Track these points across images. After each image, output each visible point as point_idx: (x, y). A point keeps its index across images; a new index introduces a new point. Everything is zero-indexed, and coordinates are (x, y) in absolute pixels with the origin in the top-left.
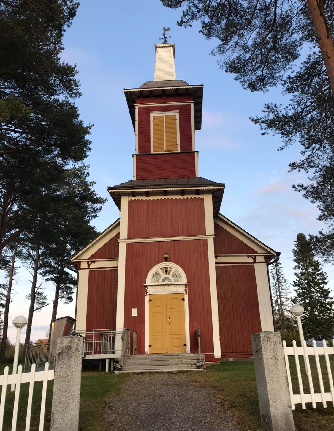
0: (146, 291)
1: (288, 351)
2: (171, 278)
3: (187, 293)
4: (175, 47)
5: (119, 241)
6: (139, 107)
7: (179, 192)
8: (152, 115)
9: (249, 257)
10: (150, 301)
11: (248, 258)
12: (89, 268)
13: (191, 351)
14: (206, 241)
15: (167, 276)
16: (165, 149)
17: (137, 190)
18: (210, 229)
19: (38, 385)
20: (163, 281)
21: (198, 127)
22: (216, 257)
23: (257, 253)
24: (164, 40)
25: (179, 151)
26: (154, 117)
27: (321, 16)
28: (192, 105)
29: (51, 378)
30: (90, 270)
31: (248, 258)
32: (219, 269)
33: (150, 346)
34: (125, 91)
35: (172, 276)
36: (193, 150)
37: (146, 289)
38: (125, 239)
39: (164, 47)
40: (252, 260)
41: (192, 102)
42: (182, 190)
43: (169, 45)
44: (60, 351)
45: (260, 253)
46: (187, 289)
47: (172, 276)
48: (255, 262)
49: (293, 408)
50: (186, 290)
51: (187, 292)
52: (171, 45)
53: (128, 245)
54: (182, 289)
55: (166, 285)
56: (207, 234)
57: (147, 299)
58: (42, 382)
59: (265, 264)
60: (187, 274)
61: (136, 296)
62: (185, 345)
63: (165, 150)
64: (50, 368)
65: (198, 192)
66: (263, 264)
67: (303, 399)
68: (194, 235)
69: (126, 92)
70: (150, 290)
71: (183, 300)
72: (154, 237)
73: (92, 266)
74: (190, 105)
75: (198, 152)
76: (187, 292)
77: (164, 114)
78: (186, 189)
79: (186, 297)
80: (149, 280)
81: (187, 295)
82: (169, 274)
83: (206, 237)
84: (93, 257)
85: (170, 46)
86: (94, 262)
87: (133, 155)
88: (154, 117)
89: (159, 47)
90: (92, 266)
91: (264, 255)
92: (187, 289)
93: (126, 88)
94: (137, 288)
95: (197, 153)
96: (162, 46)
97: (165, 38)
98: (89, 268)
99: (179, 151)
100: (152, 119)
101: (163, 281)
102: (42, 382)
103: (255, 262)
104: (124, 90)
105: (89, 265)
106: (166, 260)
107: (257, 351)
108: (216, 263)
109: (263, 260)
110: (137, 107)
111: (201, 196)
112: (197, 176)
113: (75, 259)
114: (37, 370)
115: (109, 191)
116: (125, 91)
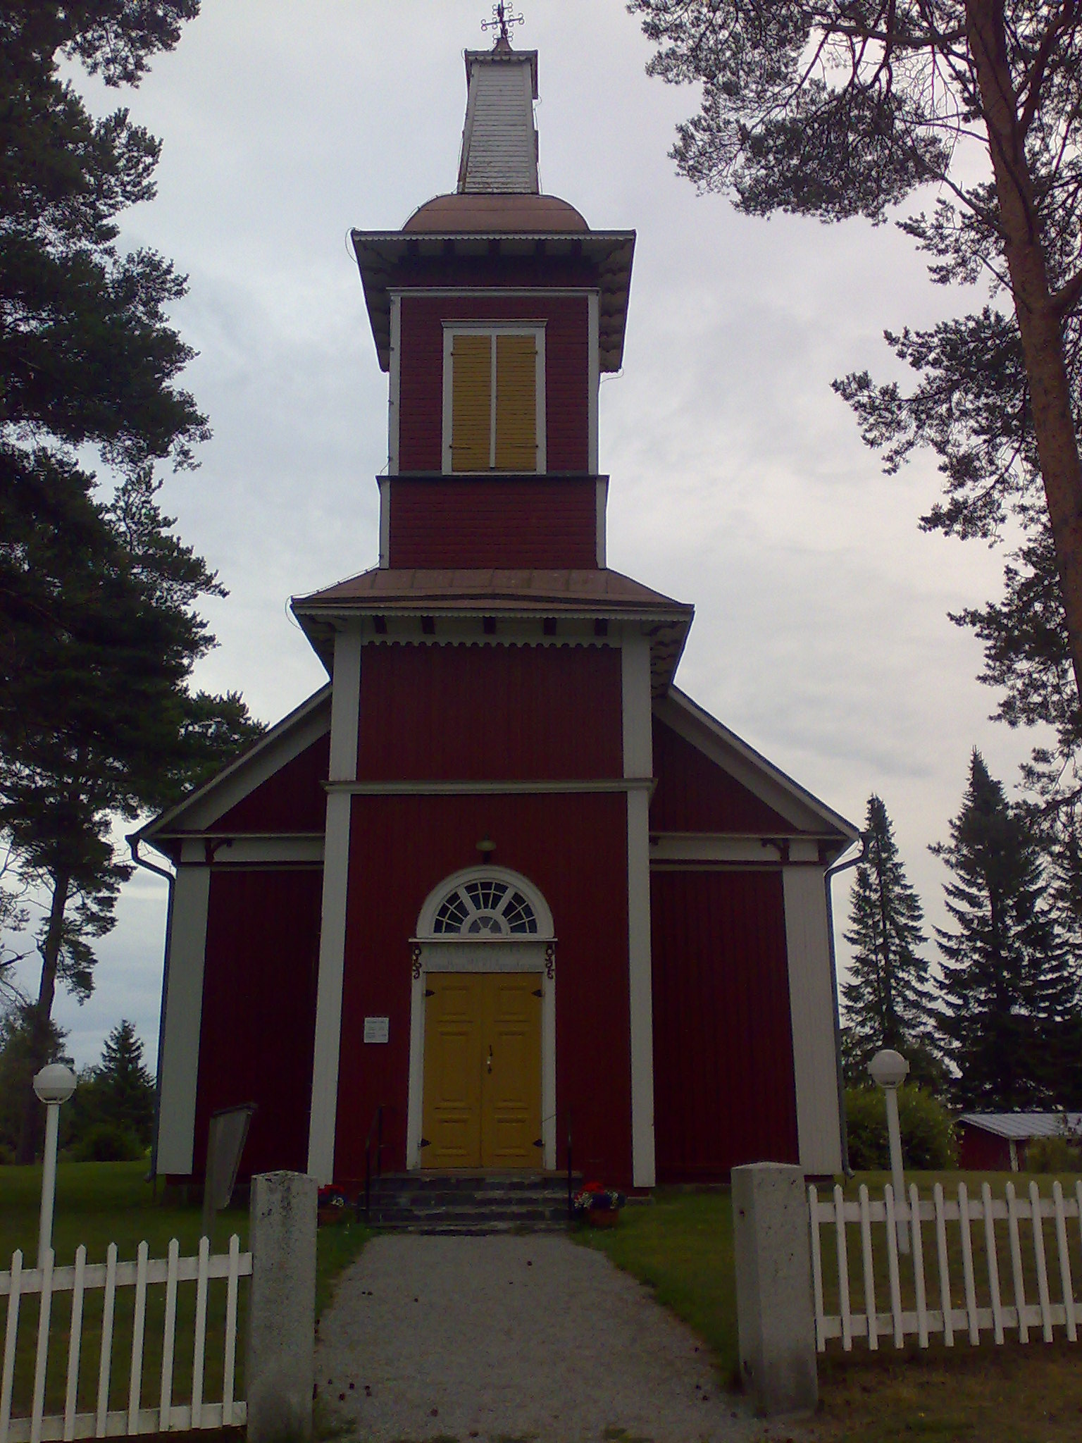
1: (820, 1212)
2: (503, 921)
3: (553, 974)
5: (327, 788)
9: (765, 842)
10: (429, 993)
11: (764, 845)
15: (488, 912)
16: (493, 460)
18: (638, 754)
19: (218, 1286)
20: (474, 928)
21: (612, 363)
22: (653, 840)
25: (541, 469)
30: (214, 869)
31: (764, 845)
32: (660, 880)
33: (424, 1143)
35: (505, 913)
37: (417, 956)
38: (346, 783)
40: (771, 855)
45: (803, 832)
47: (505, 913)
48: (785, 861)
49: (822, 1347)
53: (358, 801)
54: (536, 961)
57: (418, 988)
58: (172, 1404)
60: (428, 207)
61: (381, 974)
62: (539, 1143)
63: (492, 465)
64: (243, 1249)
67: (849, 1327)
68: (580, 776)
70: (429, 961)
71: (539, 993)
72: (445, 776)
73: (222, 855)
77: (492, 332)
79: (549, 987)
80: (424, 930)
84: (224, 823)
86: (229, 842)
90: (222, 855)
94: (534, 1195)
97: (501, 21)
98: (209, 862)
99: (541, 469)
100: (448, 346)
102: (172, 1404)
103: (785, 861)
104: (354, 233)
105: (209, 854)
106: (487, 859)
107: (742, 1213)
108: (651, 861)
110: (396, 299)
114: (213, 1250)
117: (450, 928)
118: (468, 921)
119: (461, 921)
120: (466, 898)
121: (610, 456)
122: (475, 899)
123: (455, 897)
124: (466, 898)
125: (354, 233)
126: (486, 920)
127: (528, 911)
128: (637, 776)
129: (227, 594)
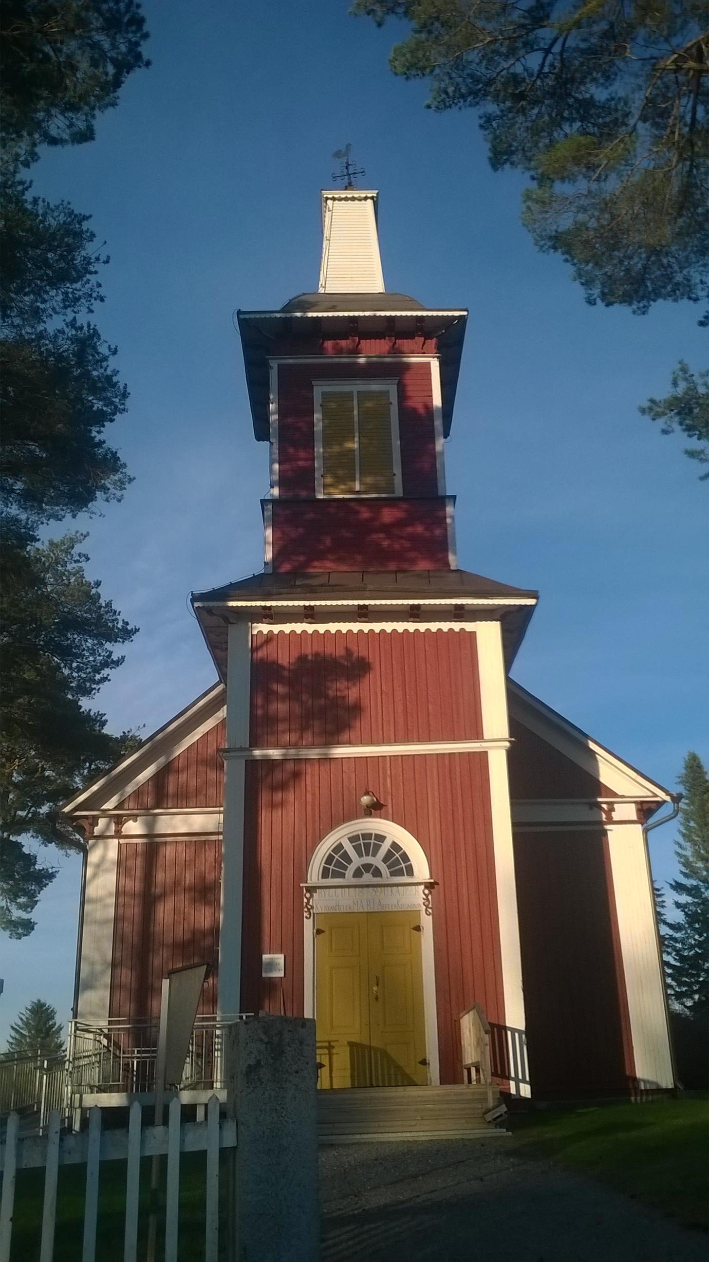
0: (308, 903)
4: (380, 200)
6: (280, 366)
7: (450, 611)
8: (319, 390)
10: (319, 932)
12: (118, 835)
13: (443, 1081)
14: (483, 757)
17: (280, 603)
23: (615, 795)
24: (346, 181)
26: (324, 394)
27: (645, 122)
28: (435, 365)
29: (230, 1141)
30: (122, 841)
34: (242, 316)
36: (440, 493)
37: (308, 900)
39: (346, 199)
41: (434, 357)
42: (456, 606)
43: (364, 196)
44: (252, 1062)
45: (623, 797)
46: (430, 897)
50: (428, 900)
51: (430, 906)
52: (370, 195)
55: (368, 886)
56: (485, 737)
57: (308, 926)
58: (204, 1152)
59: (639, 827)
62: (424, 1062)
65: (459, 614)
66: (633, 825)
69: (245, 319)
70: (320, 902)
71: (418, 928)
74: (429, 364)
75: (454, 497)
76: (430, 906)
78: (372, 602)
81: (431, 917)
82: (374, 855)
83: (484, 744)
85: (366, 198)
87: (263, 502)
88: (324, 394)
89: (334, 199)
91: (635, 802)
92: (430, 897)
93: (243, 310)
95: (452, 500)
96: (343, 196)
101: (358, 873)
102: (204, 1152)
104: (239, 312)
109: (634, 817)
110: (274, 364)
111: (469, 626)
112: (452, 568)
113: (76, 809)
115: (196, 605)
116: (242, 316)
117: (337, 875)
118: (351, 869)
119: (346, 868)
120: (348, 847)
121: (452, 482)
122: (357, 849)
123: (340, 847)
124: (348, 847)
125: (239, 312)
126: (367, 867)
127: (329, 860)
128: (495, 737)
129: (88, 533)
